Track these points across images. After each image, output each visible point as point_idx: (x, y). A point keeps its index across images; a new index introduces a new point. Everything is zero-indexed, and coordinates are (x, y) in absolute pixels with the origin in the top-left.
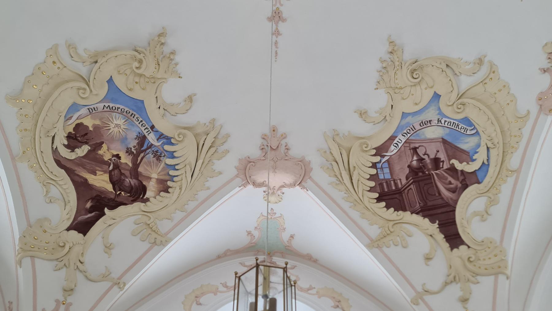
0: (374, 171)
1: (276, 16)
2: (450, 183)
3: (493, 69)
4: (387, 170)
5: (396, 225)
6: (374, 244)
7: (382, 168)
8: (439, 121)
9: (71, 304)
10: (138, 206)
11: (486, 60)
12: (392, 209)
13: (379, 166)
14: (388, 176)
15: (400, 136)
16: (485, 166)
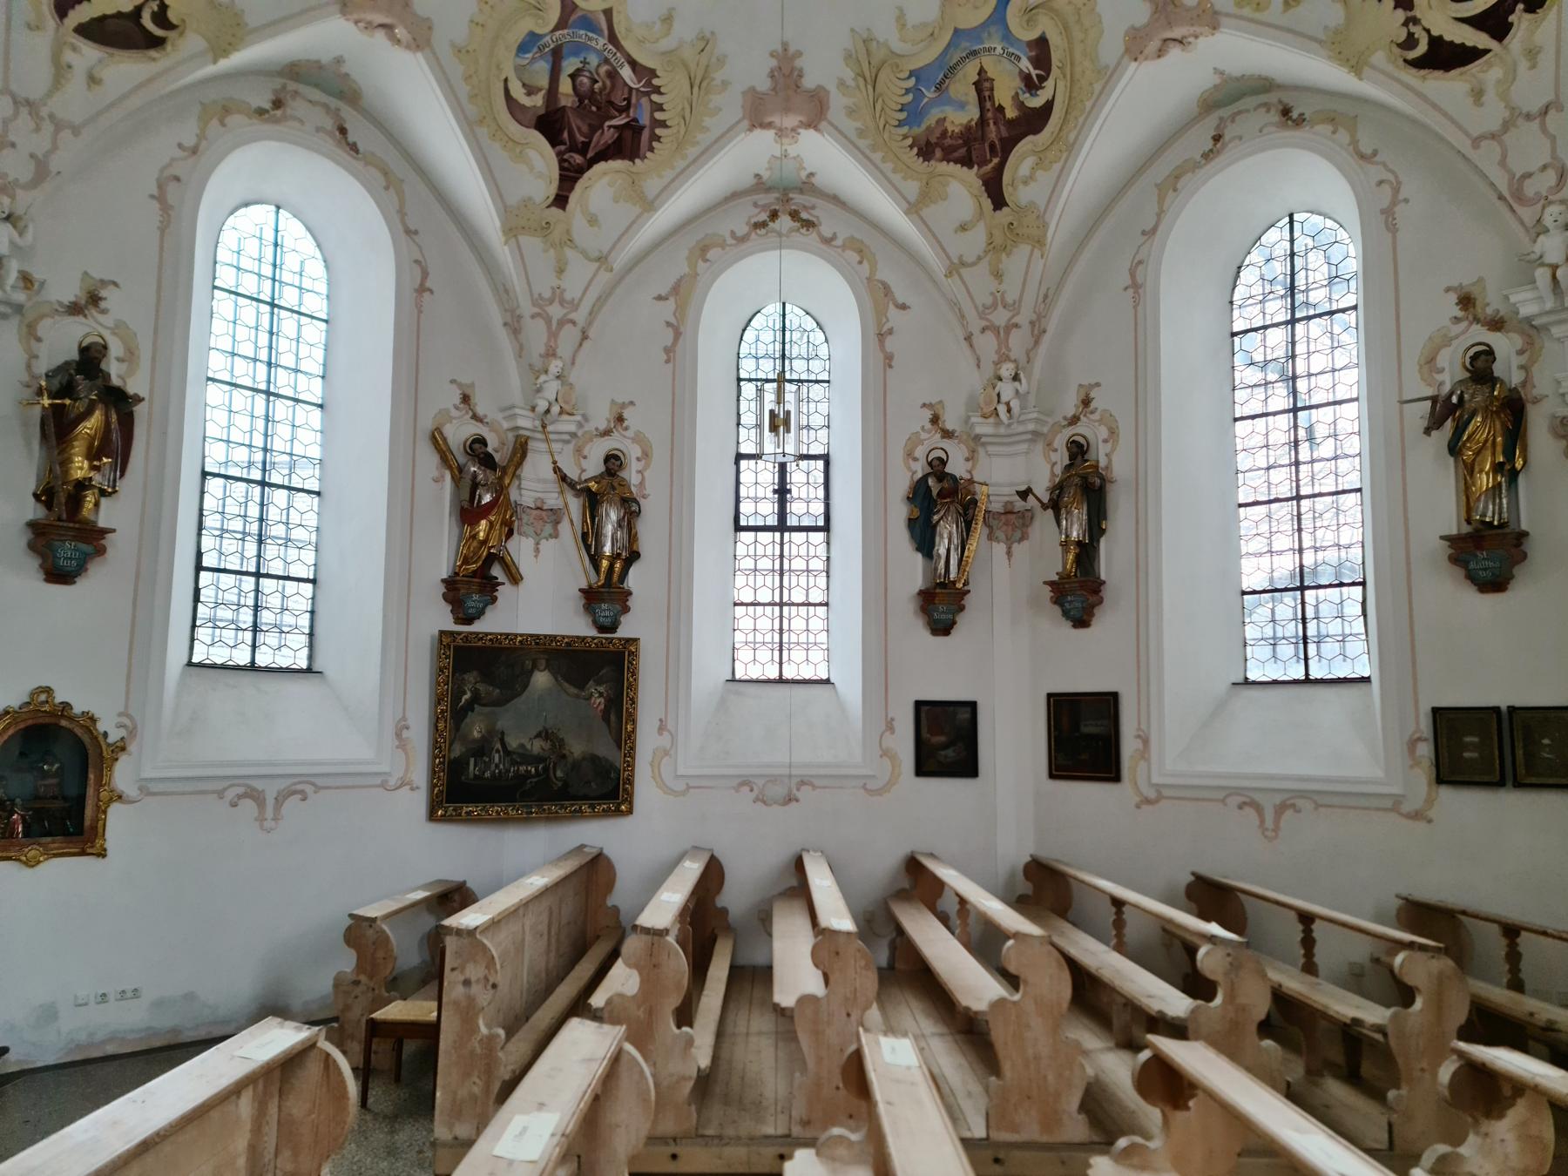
6: (913, 209)
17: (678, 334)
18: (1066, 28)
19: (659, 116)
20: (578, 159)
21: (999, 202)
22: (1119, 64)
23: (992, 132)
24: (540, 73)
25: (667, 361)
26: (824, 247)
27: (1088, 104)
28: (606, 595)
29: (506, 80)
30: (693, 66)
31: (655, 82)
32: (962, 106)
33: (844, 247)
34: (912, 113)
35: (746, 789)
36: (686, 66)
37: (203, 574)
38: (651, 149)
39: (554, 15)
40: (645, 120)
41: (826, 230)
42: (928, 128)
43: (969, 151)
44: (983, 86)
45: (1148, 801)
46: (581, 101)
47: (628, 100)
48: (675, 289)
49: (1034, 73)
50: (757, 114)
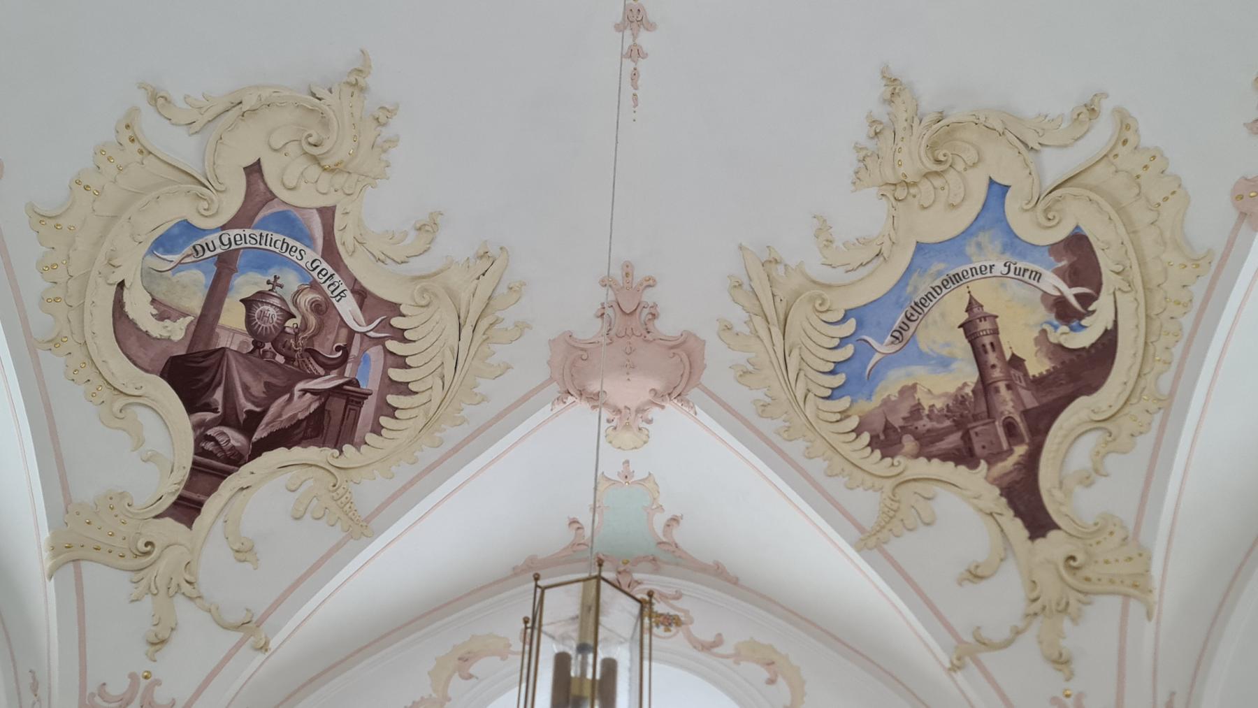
1: (635, 19)
3: (1125, 123)
5: (903, 487)
6: (871, 540)
11: (1106, 106)
18: (1119, 209)
19: (397, 375)
20: (235, 439)
21: (1038, 523)
22: (1230, 244)
23: (1007, 404)
24: (191, 289)
26: (702, 656)
27: (1187, 322)
29: (121, 285)
30: (464, 296)
31: (397, 322)
32: (944, 363)
33: (737, 657)
34: (852, 376)
36: (453, 296)
38: (377, 429)
39: (232, 203)
40: (371, 383)
41: (703, 629)
42: (886, 402)
43: (966, 438)
44: (977, 331)
46: (257, 345)
47: (346, 350)
49: (1070, 293)
50: (574, 373)
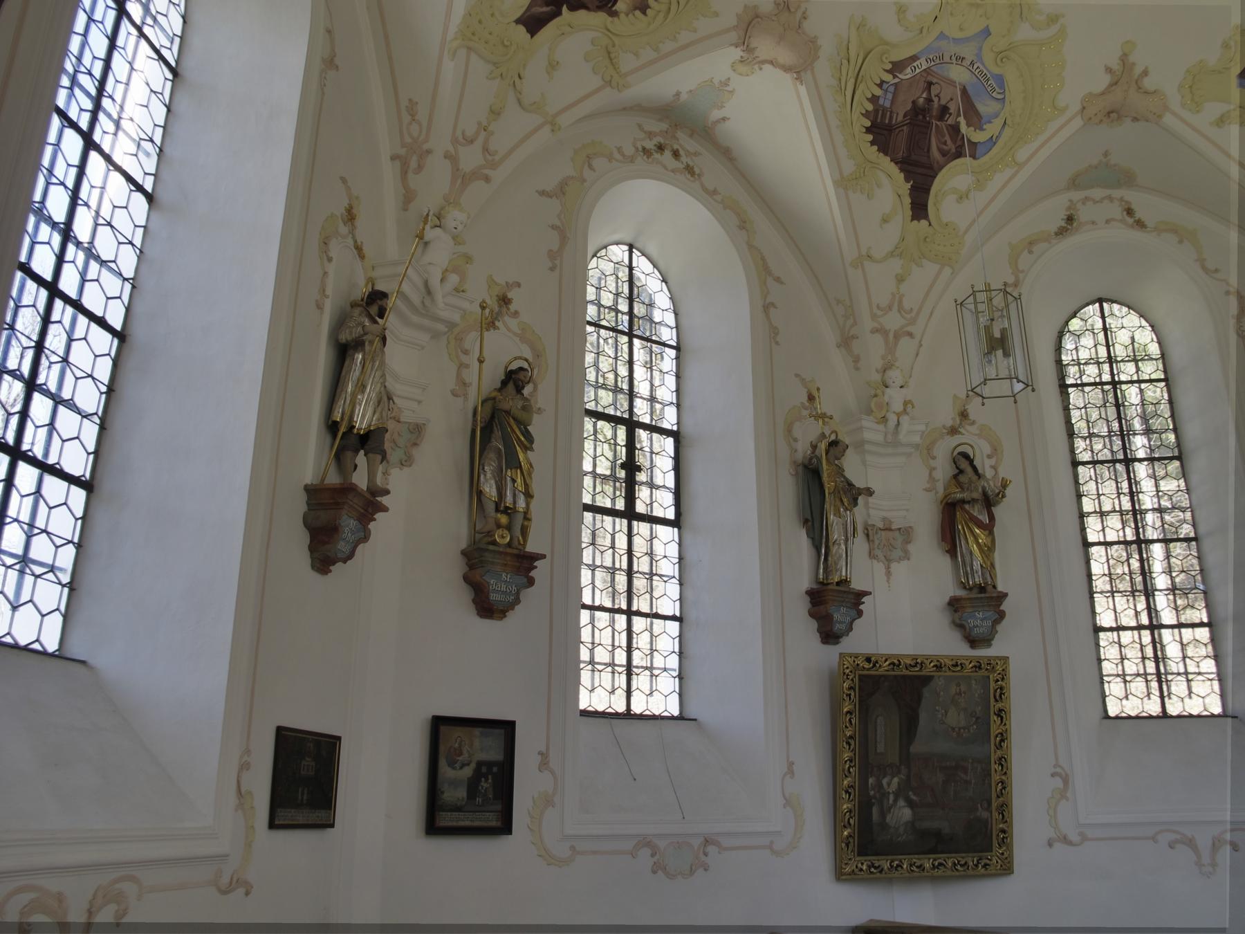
0: (878, 92)
2: (945, 143)
4: (890, 96)
6: (844, 183)
7: (886, 91)
8: (972, 63)
9: (492, 133)
10: (600, 18)
12: (875, 148)
13: (885, 86)
14: (887, 104)
15: (923, 60)
16: (992, 142)
17: (564, 239)
25: (552, 269)
28: (977, 605)
35: (646, 852)
37: (1081, 469)
45: (1065, 840)
48: (561, 191)
